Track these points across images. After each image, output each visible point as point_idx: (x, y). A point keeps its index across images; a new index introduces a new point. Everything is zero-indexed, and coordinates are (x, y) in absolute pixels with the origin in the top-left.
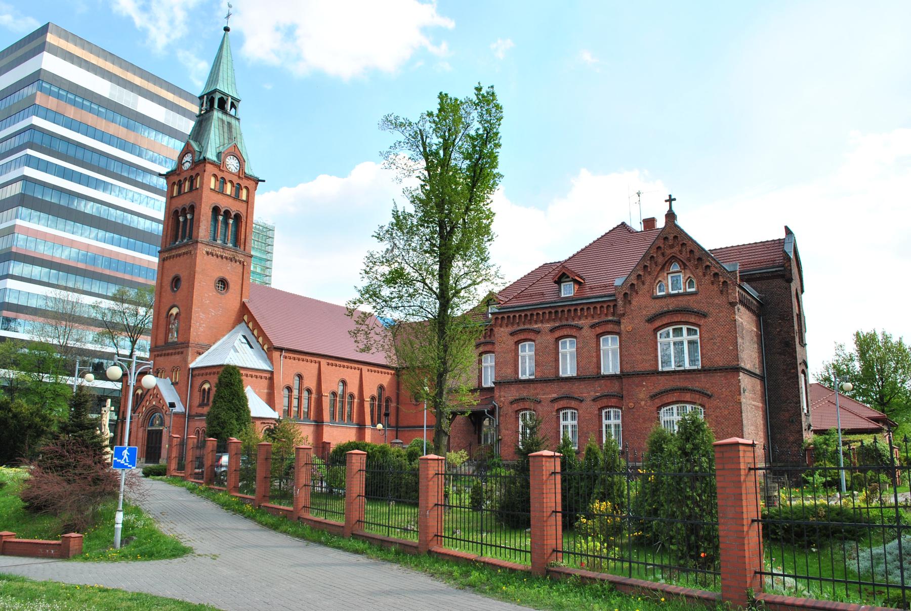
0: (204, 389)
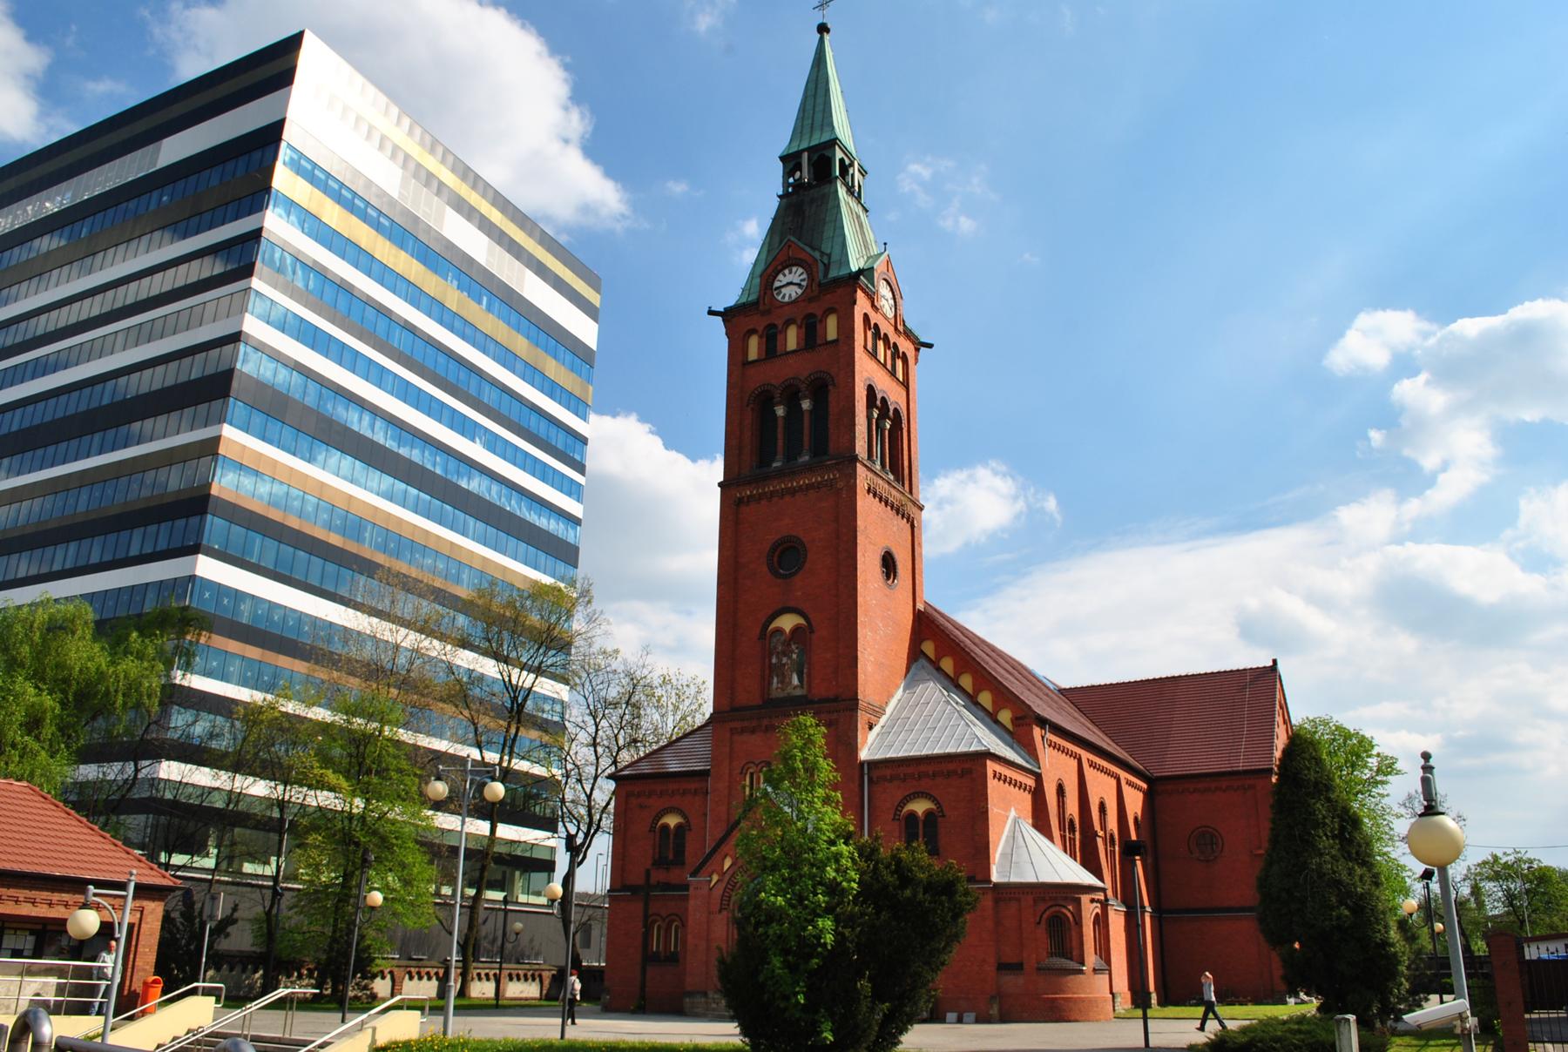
0: (666, 826)
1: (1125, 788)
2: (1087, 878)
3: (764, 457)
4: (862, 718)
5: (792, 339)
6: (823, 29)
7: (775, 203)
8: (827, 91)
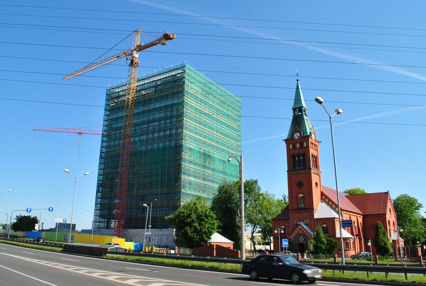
1: (358, 218)
2: (352, 236)
3: (295, 167)
4: (314, 211)
5: (298, 146)
6: (298, 80)
7: (292, 118)
8: (300, 95)
